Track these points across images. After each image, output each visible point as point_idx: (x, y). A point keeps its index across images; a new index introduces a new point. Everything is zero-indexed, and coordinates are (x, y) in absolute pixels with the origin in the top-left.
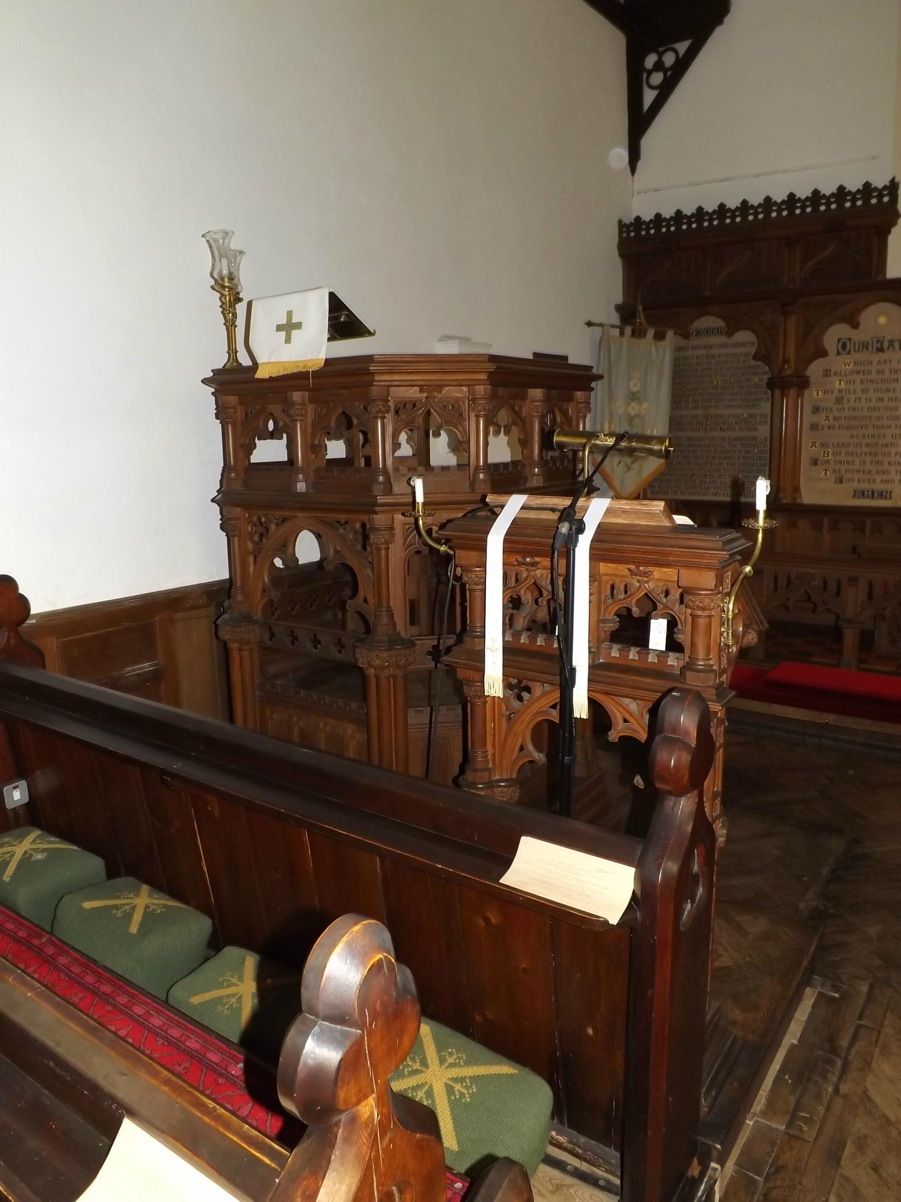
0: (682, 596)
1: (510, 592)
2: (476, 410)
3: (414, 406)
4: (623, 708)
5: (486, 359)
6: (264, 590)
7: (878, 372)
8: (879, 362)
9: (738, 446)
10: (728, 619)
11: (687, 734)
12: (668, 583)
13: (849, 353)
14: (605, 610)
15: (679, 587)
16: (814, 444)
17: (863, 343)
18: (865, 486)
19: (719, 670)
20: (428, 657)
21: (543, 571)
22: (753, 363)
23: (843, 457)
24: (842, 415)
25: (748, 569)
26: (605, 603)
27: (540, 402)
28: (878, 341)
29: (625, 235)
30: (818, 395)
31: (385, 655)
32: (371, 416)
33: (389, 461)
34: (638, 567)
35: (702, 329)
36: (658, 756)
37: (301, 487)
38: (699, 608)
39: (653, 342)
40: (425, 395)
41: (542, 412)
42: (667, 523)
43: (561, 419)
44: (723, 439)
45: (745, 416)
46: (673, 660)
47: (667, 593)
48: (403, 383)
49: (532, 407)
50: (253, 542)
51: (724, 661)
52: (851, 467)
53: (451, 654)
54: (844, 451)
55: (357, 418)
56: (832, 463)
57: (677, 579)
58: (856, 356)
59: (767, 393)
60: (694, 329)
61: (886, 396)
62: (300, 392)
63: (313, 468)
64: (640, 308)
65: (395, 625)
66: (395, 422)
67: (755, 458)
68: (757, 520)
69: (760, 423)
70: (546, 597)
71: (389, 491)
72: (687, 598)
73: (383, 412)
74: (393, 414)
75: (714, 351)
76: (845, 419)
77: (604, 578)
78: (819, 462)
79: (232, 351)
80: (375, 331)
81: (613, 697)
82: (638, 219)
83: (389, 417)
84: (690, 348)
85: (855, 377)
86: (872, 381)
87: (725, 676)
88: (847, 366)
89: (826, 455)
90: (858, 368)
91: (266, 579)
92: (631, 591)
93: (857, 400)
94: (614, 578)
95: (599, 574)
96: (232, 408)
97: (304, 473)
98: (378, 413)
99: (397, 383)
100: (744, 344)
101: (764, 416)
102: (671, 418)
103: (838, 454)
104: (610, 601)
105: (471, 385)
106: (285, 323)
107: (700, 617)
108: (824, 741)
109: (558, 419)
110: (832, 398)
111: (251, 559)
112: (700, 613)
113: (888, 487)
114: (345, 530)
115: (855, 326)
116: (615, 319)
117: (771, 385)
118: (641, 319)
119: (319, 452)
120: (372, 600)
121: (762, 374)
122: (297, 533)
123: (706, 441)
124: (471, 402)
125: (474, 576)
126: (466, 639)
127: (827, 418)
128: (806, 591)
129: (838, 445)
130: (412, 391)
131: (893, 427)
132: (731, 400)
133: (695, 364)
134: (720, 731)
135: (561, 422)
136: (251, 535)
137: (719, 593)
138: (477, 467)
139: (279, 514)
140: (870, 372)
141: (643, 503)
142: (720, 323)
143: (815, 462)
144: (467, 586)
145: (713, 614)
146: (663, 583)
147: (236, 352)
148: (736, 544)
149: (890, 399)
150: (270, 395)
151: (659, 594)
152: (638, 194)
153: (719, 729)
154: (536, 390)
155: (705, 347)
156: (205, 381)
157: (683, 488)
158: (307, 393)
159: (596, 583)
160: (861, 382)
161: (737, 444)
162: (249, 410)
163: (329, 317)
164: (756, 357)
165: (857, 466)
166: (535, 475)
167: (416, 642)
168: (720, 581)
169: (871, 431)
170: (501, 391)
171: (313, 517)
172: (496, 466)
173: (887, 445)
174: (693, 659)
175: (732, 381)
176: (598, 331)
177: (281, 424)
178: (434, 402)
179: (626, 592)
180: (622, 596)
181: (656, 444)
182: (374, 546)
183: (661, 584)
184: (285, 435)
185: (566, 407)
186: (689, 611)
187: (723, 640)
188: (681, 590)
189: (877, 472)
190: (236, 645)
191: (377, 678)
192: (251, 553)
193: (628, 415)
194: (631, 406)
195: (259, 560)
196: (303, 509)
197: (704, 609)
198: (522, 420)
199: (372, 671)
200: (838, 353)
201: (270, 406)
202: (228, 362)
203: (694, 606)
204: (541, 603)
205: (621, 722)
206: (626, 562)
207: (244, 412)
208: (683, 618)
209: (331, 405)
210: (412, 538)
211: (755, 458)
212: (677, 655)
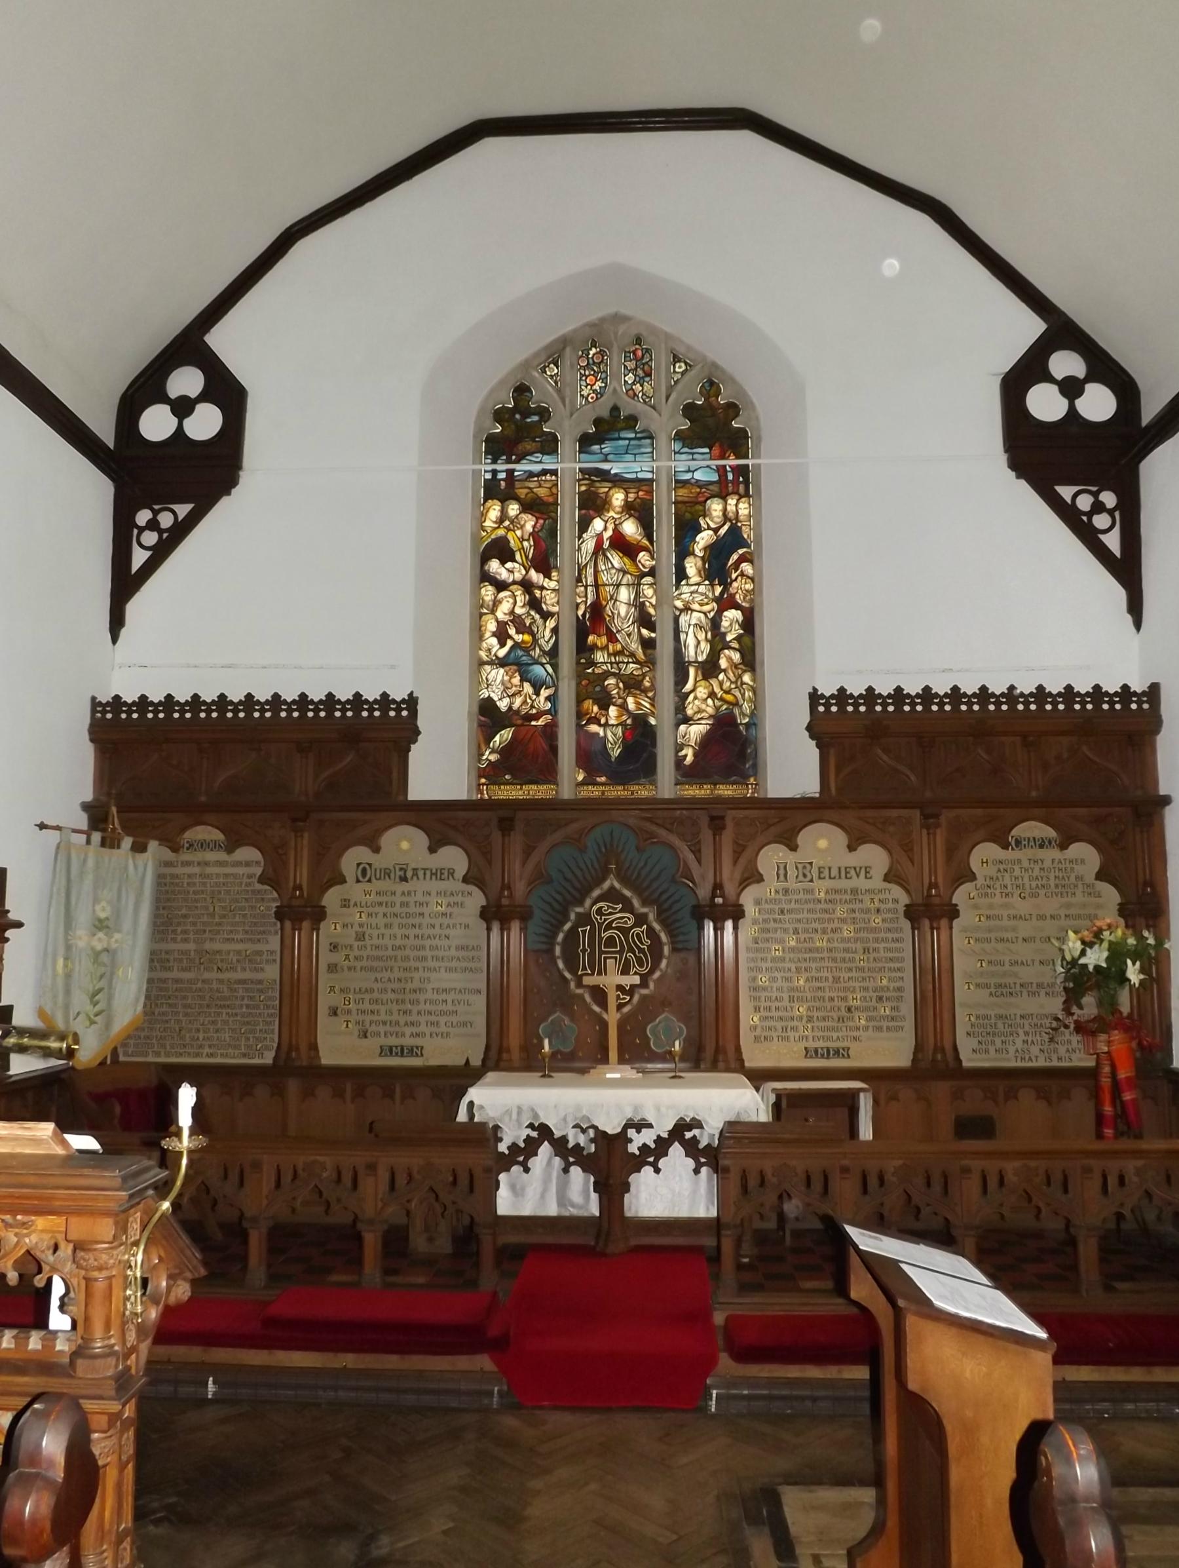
7: (403, 904)
8: (403, 893)
9: (241, 991)
10: (136, 1278)
11: (51, 1464)
12: (56, 1234)
13: (370, 881)
16: (332, 988)
17: (385, 869)
18: (393, 1041)
22: (259, 886)
23: (367, 1006)
24: (365, 954)
25: (166, 1205)
28: (401, 869)
30: (335, 929)
36: (7, 1504)
39: (130, 853)
42: (60, 1151)
44: (221, 981)
51: (131, 1337)
52: (375, 1018)
54: (367, 996)
56: (354, 1012)
57: (64, 1229)
58: (377, 885)
59: (275, 924)
61: (412, 932)
64: (114, 809)
67: (262, 1007)
68: (180, 1140)
69: (268, 961)
75: (209, 870)
76: (367, 959)
78: (339, 1012)
82: (117, 698)
85: (377, 909)
86: (395, 915)
87: (134, 1356)
88: (368, 896)
89: (347, 1003)
90: (380, 899)
92: (5, 1250)
93: (381, 936)
100: (248, 864)
101: (272, 952)
102: (153, 953)
103: (361, 1002)
107: (96, 1280)
108: (341, 1393)
110: (351, 932)
112: (96, 1274)
113: (418, 1042)
115: (377, 850)
116: (82, 821)
117: (280, 915)
118: (116, 822)
121: (271, 900)
123: (199, 985)
127: (347, 957)
128: (316, 1186)
129: (360, 990)
131: (421, 970)
132: (231, 932)
133: (185, 884)
134: (128, 1438)
137: (121, 1245)
140: (393, 904)
141: (26, 1126)
142: (218, 836)
143: (334, 1012)
145: (114, 1273)
146: (50, 1235)
148: (147, 1176)
149: (416, 937)
152: (120, 667)
155: (199, 864)
157: (168, 1047)
160: (385, 915)
164: (261, 880)
165: (383, 1017)
168: (123, 1228)
169: (397, 974)
173: (415, 991)
175: (232, 908)
176: (53, 837)
181: (55, 1041)
183: (46, 1237)
186: (83, 1272)
187: (129, 1306)
189: (406, 1024)
193: (93, 949)
194: (96, 937)
197: (100, 1269)
200: (358, 881)
203: (86, 1265)
211: (262, 1007)
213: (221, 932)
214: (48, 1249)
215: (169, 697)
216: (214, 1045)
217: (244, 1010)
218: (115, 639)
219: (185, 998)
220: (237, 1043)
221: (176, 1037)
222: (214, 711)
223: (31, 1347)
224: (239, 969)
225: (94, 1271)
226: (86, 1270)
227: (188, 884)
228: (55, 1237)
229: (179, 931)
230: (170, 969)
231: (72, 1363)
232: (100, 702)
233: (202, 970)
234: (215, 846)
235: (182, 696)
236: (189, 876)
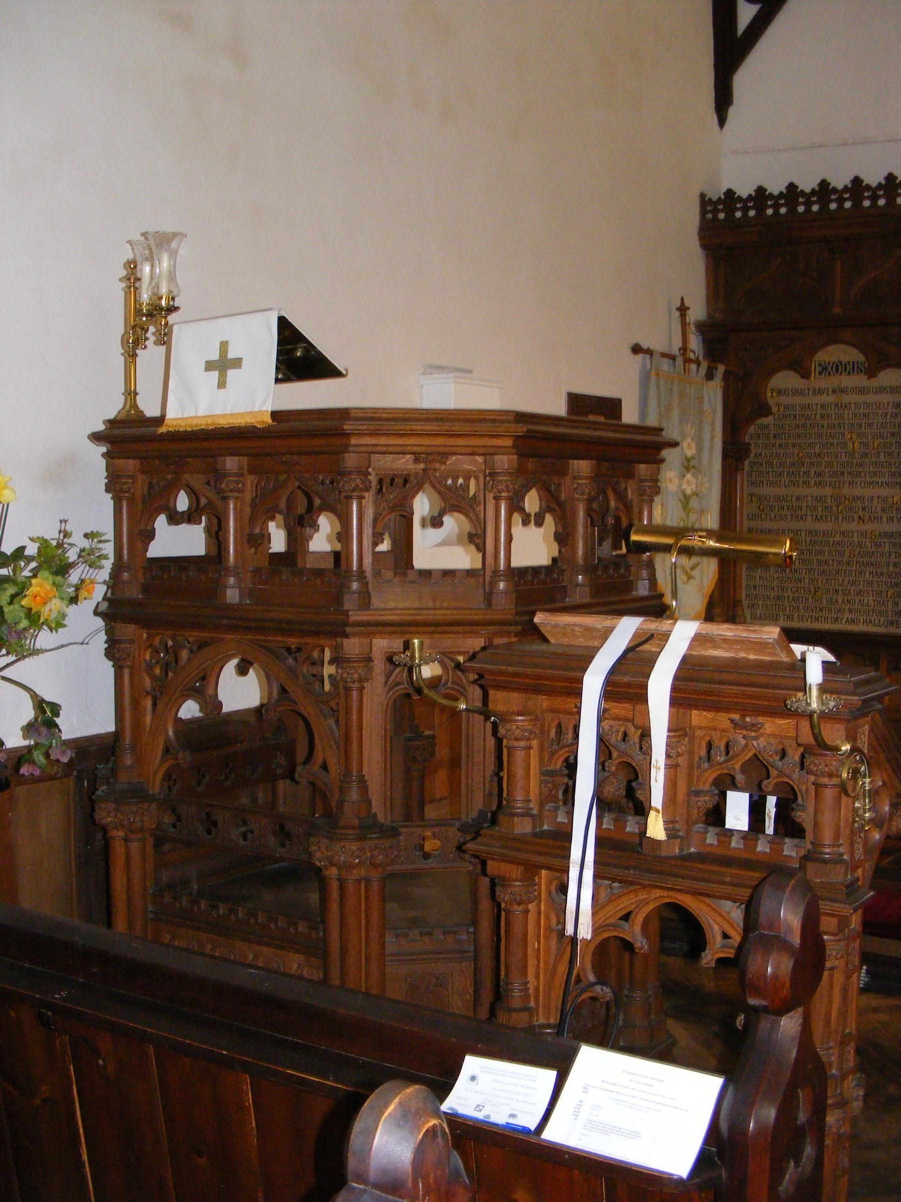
0: (803, 757)
1: (566, 752)
2: (495, 490)
3: (406, 481)
4: (722, 916)
5: (511, 418)
6: (167, 750)
14: (698, 777)
15: (799, 745)
19: (852, 862)
20: (417, 853)
21: (612, 722)
26: (699, 767)
27: (588, 479)
29: (710, 216)
31: (354, 847)
32: (343, 494)
33: (368, 561)
34: (744, 716)
35: (829, 363)
37: (232, 595)
38: (823, 774)
40: (422, 466)
41: (590, 494)
43: (615, 504)
44: (863, 534)
45: (895, 499)
46: (790, 849)
47: (783, 754)
48: (391, 449)
49: (575, 486)
50: (153, 677)
53: (479, 840)
55: (320, 498)
60: (817, 363)
62: (236, 458)
63: (251, 569)
65: (370, 803)
66: (377, 505)
70: (617, 759)
71: (365, 602)
72: (807, 761)
73: (362, 490)
74: (374, 492)
75: (846, 399)
77: (698, 733)
79: (131, 394)
80: (346, 370)
81: (707, 900)
82: (730, 193)
83: (369, 496)
84: (811, 392)
87: (860, 870)
91: (171, 733)
92: (734, 751)
94: (709, 731)
95: (691, 727)
96: (129, 477)
97: (236, 575)
98: (353, 490)
99: (384, 449)
104: (706, 764)
105: (490, 454)
106: (217, 358)
107: (826, 786)
109: (613, 504)
111: (149, 703)
114: (297, 661)
119: (260, 544)
120: (335, 769)
122: (222, 664)
123: (837, 538)
124: (488, 478)
125: (514, 727)
126: (502, 819)
130: (404, 460)
135: (617, 508)
136: (150, 667)
138: (496, 573)
139: (193, 635)
141: (751, 628)
144: (505, 742)
147: (136, 394)
150: (188, 460)
151: (771, 756)
153: (852, 945)
154: (581, 462)
155: (834, 391)
156: (96, 437)
158: (246, 458)
159: (687, 739)
161: (884, 543)
162: (155, 481)
163: (278, 351)
166: (577, 585)
167: (401, 830)
170: (531, 464)
171: (251, 640)
172: (523, 572)
174: (817, 845)
175: (876, 444)
177: (203, 501)
178: (435, 477)
179: (727, 753)
180: (721, 758)
182: (341, 684)
184: (203, 518)
185: (624, 486)
186: (812, 778)
188: (802, 749)
190: (120, 834)
191: (342, 881)
192: (148, 693)
195: (160, 704)
196: (235, 629)
198: (559, 504)
199: (333, 872)
201: (187, 476)
202: (123, 408)
203: (817, 771)
204: (609, 767)
205: (719, 938)
206: (728, 709)
207: (147, 481)
208: (804, 788)
209: (282, 477)
210: (397, 676)
212: (797, 841)
213: (863, 474)
214: (777, 753)
215: (824, 184)
216: (856, 611)
217: (891, 568)
218: (722, 121)
219: (821, 552)
220: (883, 608)
221: (810, 599)
222: (782, 205)
223: (759, 849)
224: (885, 519)
225: (823, 777)
226: (816, 775)
227: (822, 416)
228: (782, 743)
229: (812, 473)
230: (802, 518)
231: (802, 867)
232: (710, 200)
233: (840, 521)
234: (852, 368)
235: (807, 184)
236: (823, 406)
